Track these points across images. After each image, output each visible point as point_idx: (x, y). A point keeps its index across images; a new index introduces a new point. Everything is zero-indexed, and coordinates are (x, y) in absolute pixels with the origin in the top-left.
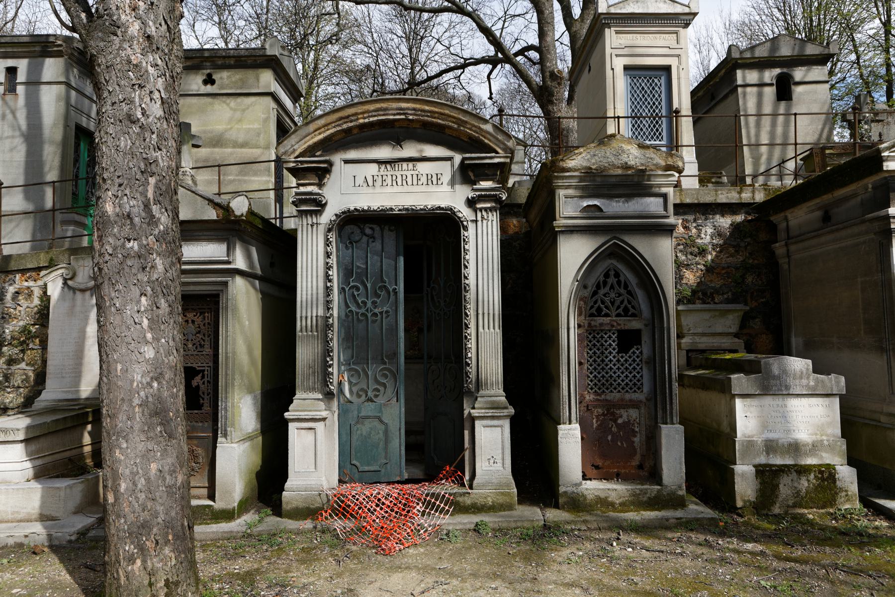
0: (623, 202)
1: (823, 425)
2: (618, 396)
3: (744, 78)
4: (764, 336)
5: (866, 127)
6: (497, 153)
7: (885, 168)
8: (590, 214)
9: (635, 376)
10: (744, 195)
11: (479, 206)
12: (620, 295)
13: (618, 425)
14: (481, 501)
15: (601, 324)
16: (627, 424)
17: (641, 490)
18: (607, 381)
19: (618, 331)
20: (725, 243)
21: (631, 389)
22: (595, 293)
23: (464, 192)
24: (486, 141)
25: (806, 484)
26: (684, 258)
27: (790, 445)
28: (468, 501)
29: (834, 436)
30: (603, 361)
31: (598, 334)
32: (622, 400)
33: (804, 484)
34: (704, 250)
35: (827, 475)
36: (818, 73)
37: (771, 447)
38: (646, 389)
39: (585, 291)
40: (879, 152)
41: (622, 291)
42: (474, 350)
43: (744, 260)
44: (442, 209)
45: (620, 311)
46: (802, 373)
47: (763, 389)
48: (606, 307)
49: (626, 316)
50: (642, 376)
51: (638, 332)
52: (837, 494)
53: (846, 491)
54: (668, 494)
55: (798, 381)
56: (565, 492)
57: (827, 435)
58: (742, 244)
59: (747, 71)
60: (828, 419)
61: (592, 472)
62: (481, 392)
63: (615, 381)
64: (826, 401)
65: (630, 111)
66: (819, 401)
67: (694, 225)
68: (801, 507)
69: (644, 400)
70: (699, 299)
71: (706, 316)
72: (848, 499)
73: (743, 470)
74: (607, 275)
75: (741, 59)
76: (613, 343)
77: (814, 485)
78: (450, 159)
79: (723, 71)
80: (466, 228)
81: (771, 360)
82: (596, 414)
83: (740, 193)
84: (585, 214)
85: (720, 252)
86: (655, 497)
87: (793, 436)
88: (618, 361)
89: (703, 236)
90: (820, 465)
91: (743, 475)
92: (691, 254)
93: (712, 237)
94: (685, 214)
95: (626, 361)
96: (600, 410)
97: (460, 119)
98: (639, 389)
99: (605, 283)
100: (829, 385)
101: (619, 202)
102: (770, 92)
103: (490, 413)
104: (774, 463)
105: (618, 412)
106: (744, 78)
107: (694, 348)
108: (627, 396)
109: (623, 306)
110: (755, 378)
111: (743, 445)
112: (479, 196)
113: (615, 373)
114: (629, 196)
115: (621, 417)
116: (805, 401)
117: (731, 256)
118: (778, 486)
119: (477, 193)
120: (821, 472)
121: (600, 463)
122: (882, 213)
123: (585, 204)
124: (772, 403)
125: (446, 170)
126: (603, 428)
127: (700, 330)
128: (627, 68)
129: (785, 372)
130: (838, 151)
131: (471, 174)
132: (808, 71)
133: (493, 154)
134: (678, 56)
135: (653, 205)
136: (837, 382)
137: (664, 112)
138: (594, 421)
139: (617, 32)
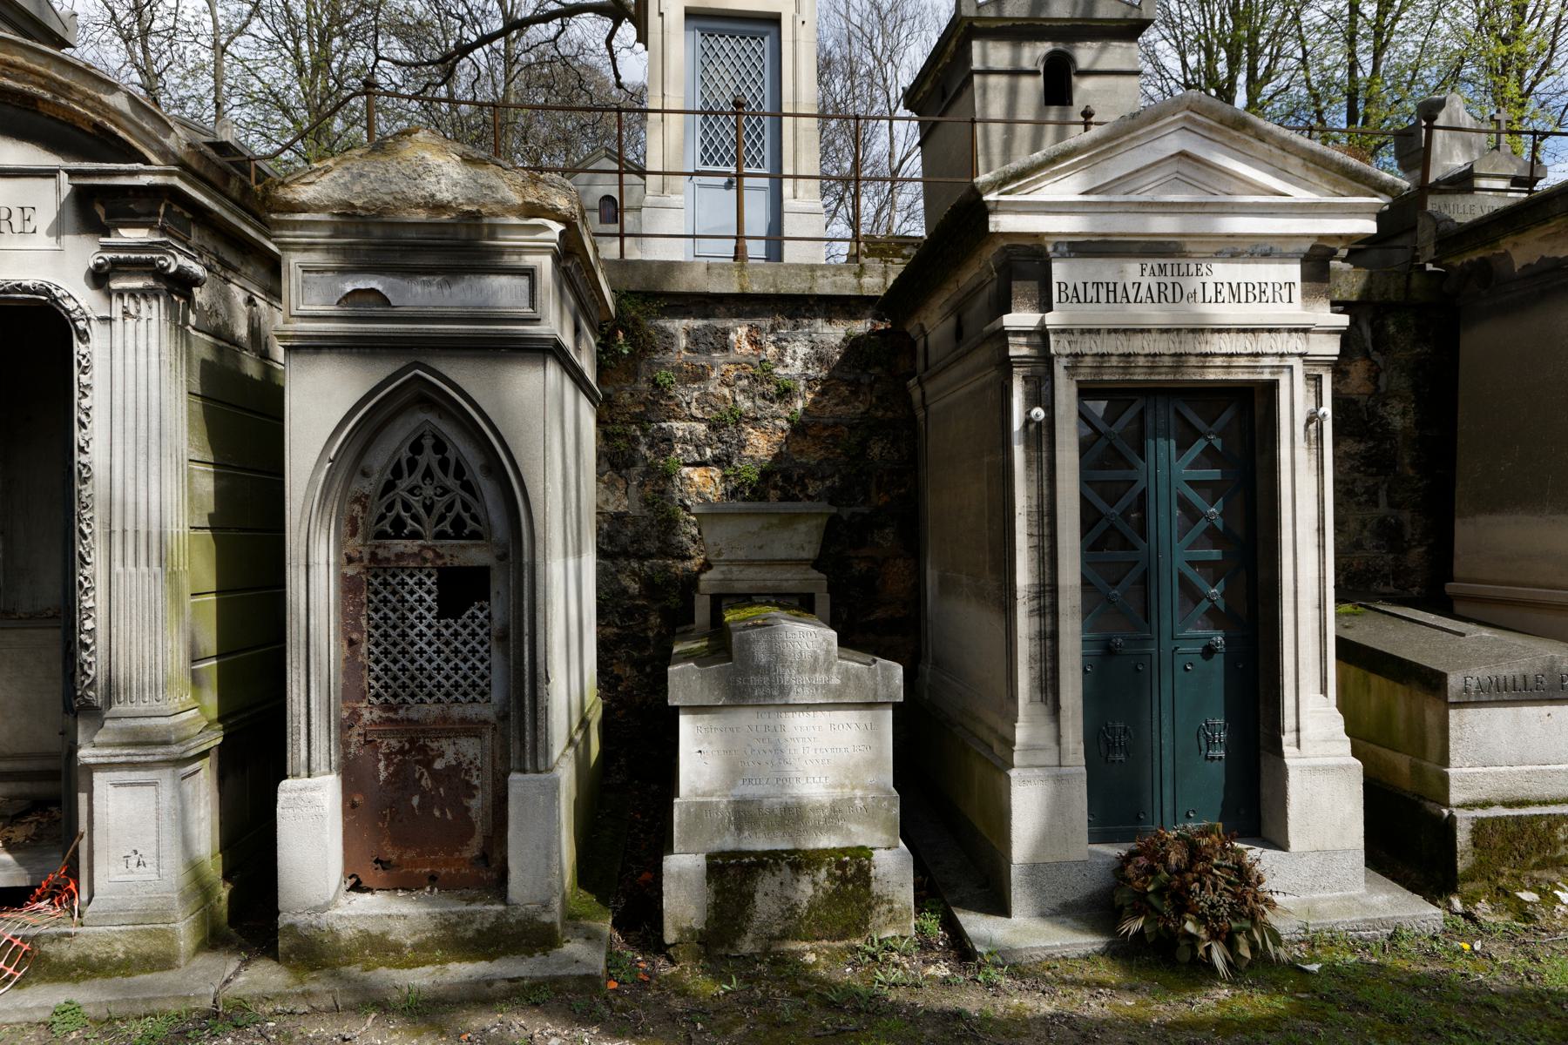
0: (440, 285)
1: (856, 766)
2: (436, 710)
4: (900, 562)
6: (147, 162)
7: (992, 229)
8: (363, 311)
9: (474, 668)
10: (866, 280)
11: (116, 285)
12: (446, 491)
13: (435, 775)
14: (98, 951)
16: (454, 771)
17: (460, 916)
18: (413, 678)
19: (439, 569)
20: (830, 377)
21: (465, 694)
22: (389, 487)
23: (85, 252)
24: (121, 134)
25: (810, 891)
26: (749, 404)
27: (787, 809)
28: (69, 952)
29: (878, 788)
30: (404, 635)
31: (394, 576)
32: (445, 719)
33: (806, 890)
34: (788, 390)
35: (853, 871)
36: (1117, 54)
38: (496, 695)
39: (365, 483)
40: (975, 194)
41: (450, 482)
42: (101, 613)
43: (867, 412)
44: (26, 290)
45: (446, 526)
46: (816, 659)
47: (734, 695)
48: (416, 518)
49: (458, 536)
50: (488, 668)
51: (483, 573)
52: (870, 907)
53: (890, 902)
54: (518, 922)
55: (806, 678)
56: (292, 926)
57: (865, 788)
58: (865, 379)
59: (990, 44)
61: (369, 875)
62: (117, 708)
63: (430, 678)
64: (867, 715)
67: (772, 338)
68: (797, 937)
69: (493, 719)
70: (775, 487)
71: (754, 525)
72: (894, 917)
73: (683, 865)
74: (417, 448)
75: (979, 19)
76: (423, 594)
77: (825, 891)
78: (50, 174)
79: (953, 43)
80: (84, 336)
81: (787, 625)
82: (384, 749)
83: (859, 275)
84: (347, 311)
85: (823, 393)
88: (438, 635)
89: (788, 360)
90: (844, 851)
91: (679, 876)
92: (763, 396)
93: (805, 364)
94: (753, 314)
95: (456, 634)
96: (393, 742)
97: (54, 80)
98: (483, 694)
99: (413, 465)
100: (870, 683)
101: (430, 284)
102: (1031, 88)
103: (122, 755)
105: (435, 745)
107: (724, 591)
108: (456, 711)
109: (451, 516)
110: (719, 672)
111: (688, 813)
112: (115, 263)
113: (430, 661)
114: (452, 272)
115: (442, 755)
117: (844, 401)
118: (751, 896)
119: (108, 256)
120: (842, 865)
121: (392, 854)
122: (995, 325)
123: (349, 288)
124: (753, 723)
125: (48, 198)
126: (402, 780)
127: (741, 554)
129: (778, 657)
131: (100, 211)
132: (1102, 50)
133: (140, 166)
135: (504, 292)
137: (767, 108)
138: (381, 765)
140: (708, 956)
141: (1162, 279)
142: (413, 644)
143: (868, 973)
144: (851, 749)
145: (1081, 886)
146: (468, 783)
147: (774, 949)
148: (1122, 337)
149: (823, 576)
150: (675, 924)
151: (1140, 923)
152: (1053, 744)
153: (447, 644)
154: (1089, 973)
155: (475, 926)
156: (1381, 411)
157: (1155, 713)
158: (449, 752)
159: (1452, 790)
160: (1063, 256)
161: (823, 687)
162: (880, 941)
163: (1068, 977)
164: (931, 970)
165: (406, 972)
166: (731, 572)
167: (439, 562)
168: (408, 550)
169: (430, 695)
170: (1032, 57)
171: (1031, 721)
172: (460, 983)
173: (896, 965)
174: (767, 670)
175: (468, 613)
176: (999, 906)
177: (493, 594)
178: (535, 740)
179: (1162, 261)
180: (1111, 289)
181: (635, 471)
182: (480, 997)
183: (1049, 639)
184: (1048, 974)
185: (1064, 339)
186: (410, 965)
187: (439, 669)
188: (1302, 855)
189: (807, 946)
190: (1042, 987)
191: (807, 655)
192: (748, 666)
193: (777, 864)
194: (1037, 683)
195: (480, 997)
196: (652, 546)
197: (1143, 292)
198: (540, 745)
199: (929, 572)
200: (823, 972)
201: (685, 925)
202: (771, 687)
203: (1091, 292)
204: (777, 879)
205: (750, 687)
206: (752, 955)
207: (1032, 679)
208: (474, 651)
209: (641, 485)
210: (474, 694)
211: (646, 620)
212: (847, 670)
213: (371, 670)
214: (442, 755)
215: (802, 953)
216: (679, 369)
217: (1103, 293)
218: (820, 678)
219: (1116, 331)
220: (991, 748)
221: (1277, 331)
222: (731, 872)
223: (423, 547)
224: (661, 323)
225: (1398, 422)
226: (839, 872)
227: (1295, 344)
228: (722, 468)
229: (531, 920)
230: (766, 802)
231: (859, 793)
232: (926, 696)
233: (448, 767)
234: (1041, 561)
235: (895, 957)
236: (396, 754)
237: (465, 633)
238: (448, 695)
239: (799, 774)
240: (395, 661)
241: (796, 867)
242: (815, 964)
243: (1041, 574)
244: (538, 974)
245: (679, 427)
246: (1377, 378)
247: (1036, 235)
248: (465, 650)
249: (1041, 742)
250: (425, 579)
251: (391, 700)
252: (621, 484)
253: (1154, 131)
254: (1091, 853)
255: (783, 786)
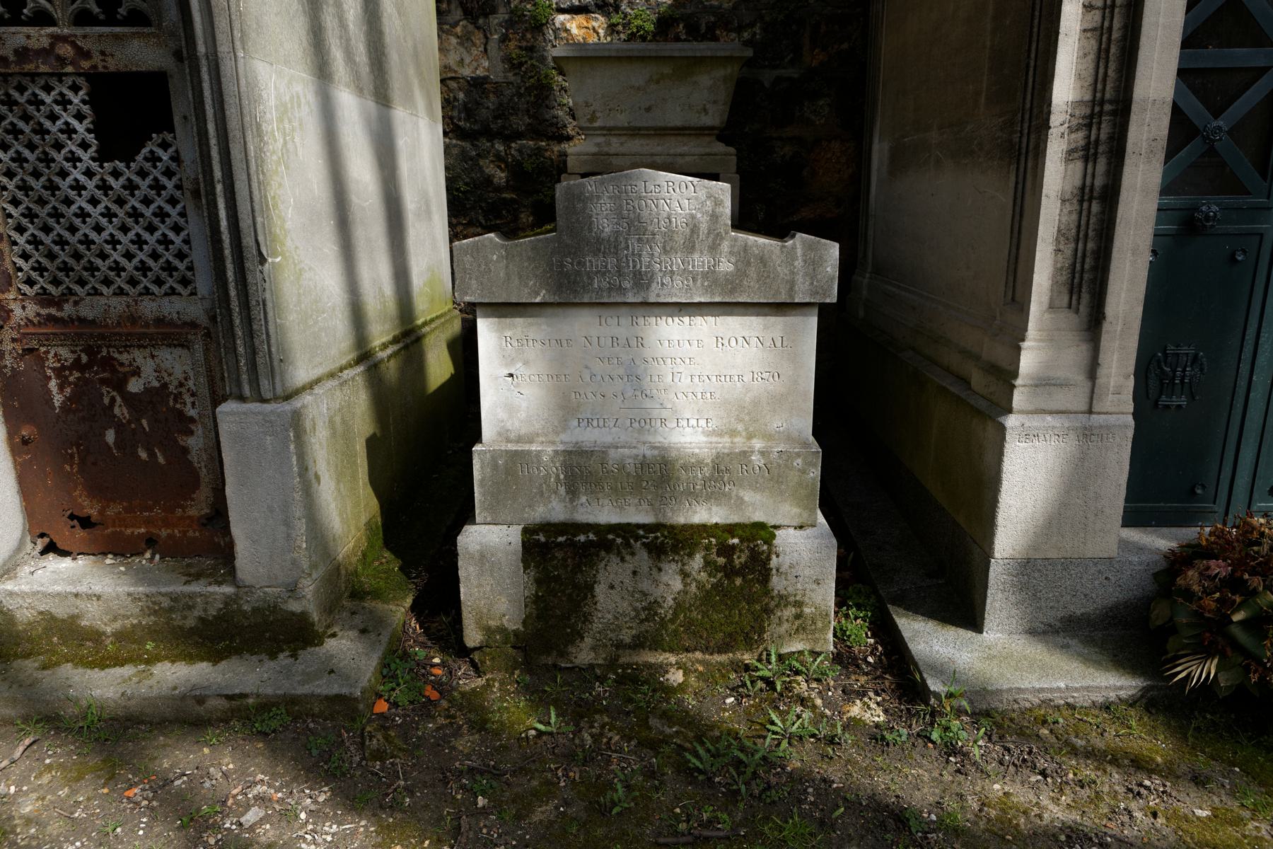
1: (756, 403)
9: (165, 241)
13: (130, 399)
15: (23, 54)
16: (157, 396)
17: (175, 598)
18: (77, 256)
21: (159, 282)
25: (677, 585)
27: (644, 464)
29: (789, 438)
30: (52, 187)
33: (672, 583)
35: (745, 555)
46: (694, 229)
47: (559, 288)
49: (111, 21)
50: (187, 242)
52: (768, 611)
53: (799, 604)
54: (255, 610)
55: (677, 261)
57: (768, 437)
60: (775, 386)
61: (66, 534)
64: (777, 324)
66: (733, 325)
68: (657, 645)
69: (203, 320)
71: (638, 75)
72: (802, 625)
76: (74, 119)
77: (700, 586)
86: (219, 618)
87: (658, 439)
88: (104, 187)
90: (731, 529)
91: (482, 557)
95: (131, 187)
96: (64, 352)
98: (185, 282)
100: (783, 271)
104: (591, 519)
105: (124, 358)
108: (148, 308)
111: (495, 467)
113: (98, 229)
115: (137, 372)
116: (705, 326)
118: (590, 588)
121: (91, 509)
127: (622, 119)
129: (635, 224)
136: (813, 262)
138: (53, 384)
140: (528, 666)
142: (68, 202)
143: (758, 707)
144: (748, 378)
145: (1100, 594)
146: (181, 415)
147: (622, 660)
149: (732, 150)
150: (478, 623)
151: (1212, 667)
152: (1080, 378)
153: (120, 202)
154: (1112, 737)
155: (196, 613)
157: (1251, 332)
158: (150, 368)
161: (705, 275)
162: (781, 658)
163: (1080, 743)
164: (856, 710)
165: (96, 674)
166: (609, 144)
167: (86, 65)
168: (34, 44)
169: (107, 282)
171: (1050, 338)
172: (159, 697)
173: (803, 701)
174: (612, 246)
175: (145, 151)
176: (967, 615)
177: (177, 120)
178: (253, 352)
181: (495, 20)
182: (189, 717)
183: (1099, 202)
184: (1045, 732)
186: (103, 663)
187: (114, 242)
189: (673, 659)
190: (1041, 763)
191: (679, 222)
192: (582, 241)
193: (628, 545)
194: (1064, 277)
195: (189, 717)
196: (520, 122)
198: (260, 360)
199: (876, 147)
200: (691, 702)
201: (492, 623)
202: (620, 273)
204: (629, 567)
205: (589, 279)
206: (591, 667)
207: (1057, 271)
208: (162, 214)
209: (504, 39)
210: (170, 282)
211: (516, 219)
212: (746, 248)
213: (15, 243)
214: (137, 372)
215: (663, 669)
218: (700, 261)
220: (966, 382)
222: (559, 555)
223: (56, 39)
226: (721, 561)
228: (607, 15)
229: (274, 608)
230: (612, 453)
231: (758, 444)
232: (861, 313)
233: (148, 390)
234: (1102, 55)
235: (802, 686)
236: (71, 368)
237: (144, 184)
238: (133, 282)
239: (665, 414)
240: (47, 229)
242: (682, 687)
243: (1097, 82)
244: (269, 691)
248: (148, 212)
249: (1061, 374)
250: (70, 95)
251: (50, 288)
252: (478, 38)
254: (1124, 544)
255: (641, 430)
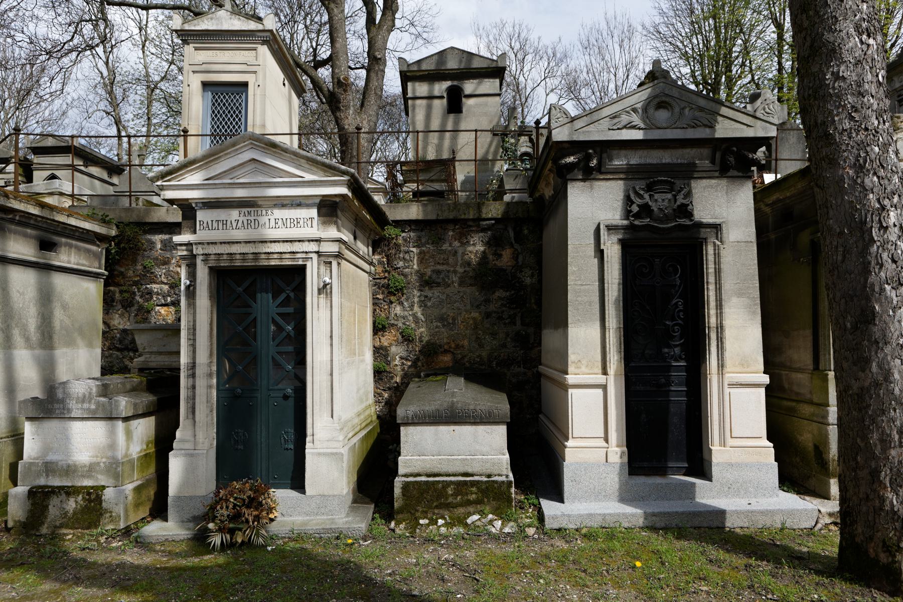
1: (104, 447)
3: (414, 90)
5: (512, 141)
33: (71, 505)
37: (49, 468)
52: (101, 514)
53: (111, 512)
57: (107, 458)
59: (417, 84)
65: (209, 126)
68: (67, 527)
72: (112, 520)
77: (81, 506)
87: (75, 459)
90: (92, 487)
91: (16, 496)
102: (439, 105)
106: (414, 90)
107: (145, 367)
118: (47, 506)
120: (89, 494)
127: (155, 349)
128: (206, 85)
130: (412, 168)
132: (479, 84)
134: (255, 72)
139: (196, 49)
141: (249, 218)
148: (227, 246)
156: (518, 275)
159: (400, 467)
160: (201, 209)
170: (440, 89)
174: (62, 401)
179: (249, 210)
180: (224, 223)
181: (133, 309)
185: (200, 247)
188: (312, 497)
191: (80, 395)
197: (240, 224)
203: (215, 225)
209: (136, 315)
216: (157, 259)
217: (220, 225)
218: (86, 406)
219: (224, 243)
221: (303, 241)
224: (149, 237)
225: (528, 281)
227: (313, 247)
230: (60, 463)
231: (104, 460)
241: (68, 494)
245: (155, 287)
246: (517, 257)
247: (187, 200)
252: (126, 315)
253: (237, 150)
